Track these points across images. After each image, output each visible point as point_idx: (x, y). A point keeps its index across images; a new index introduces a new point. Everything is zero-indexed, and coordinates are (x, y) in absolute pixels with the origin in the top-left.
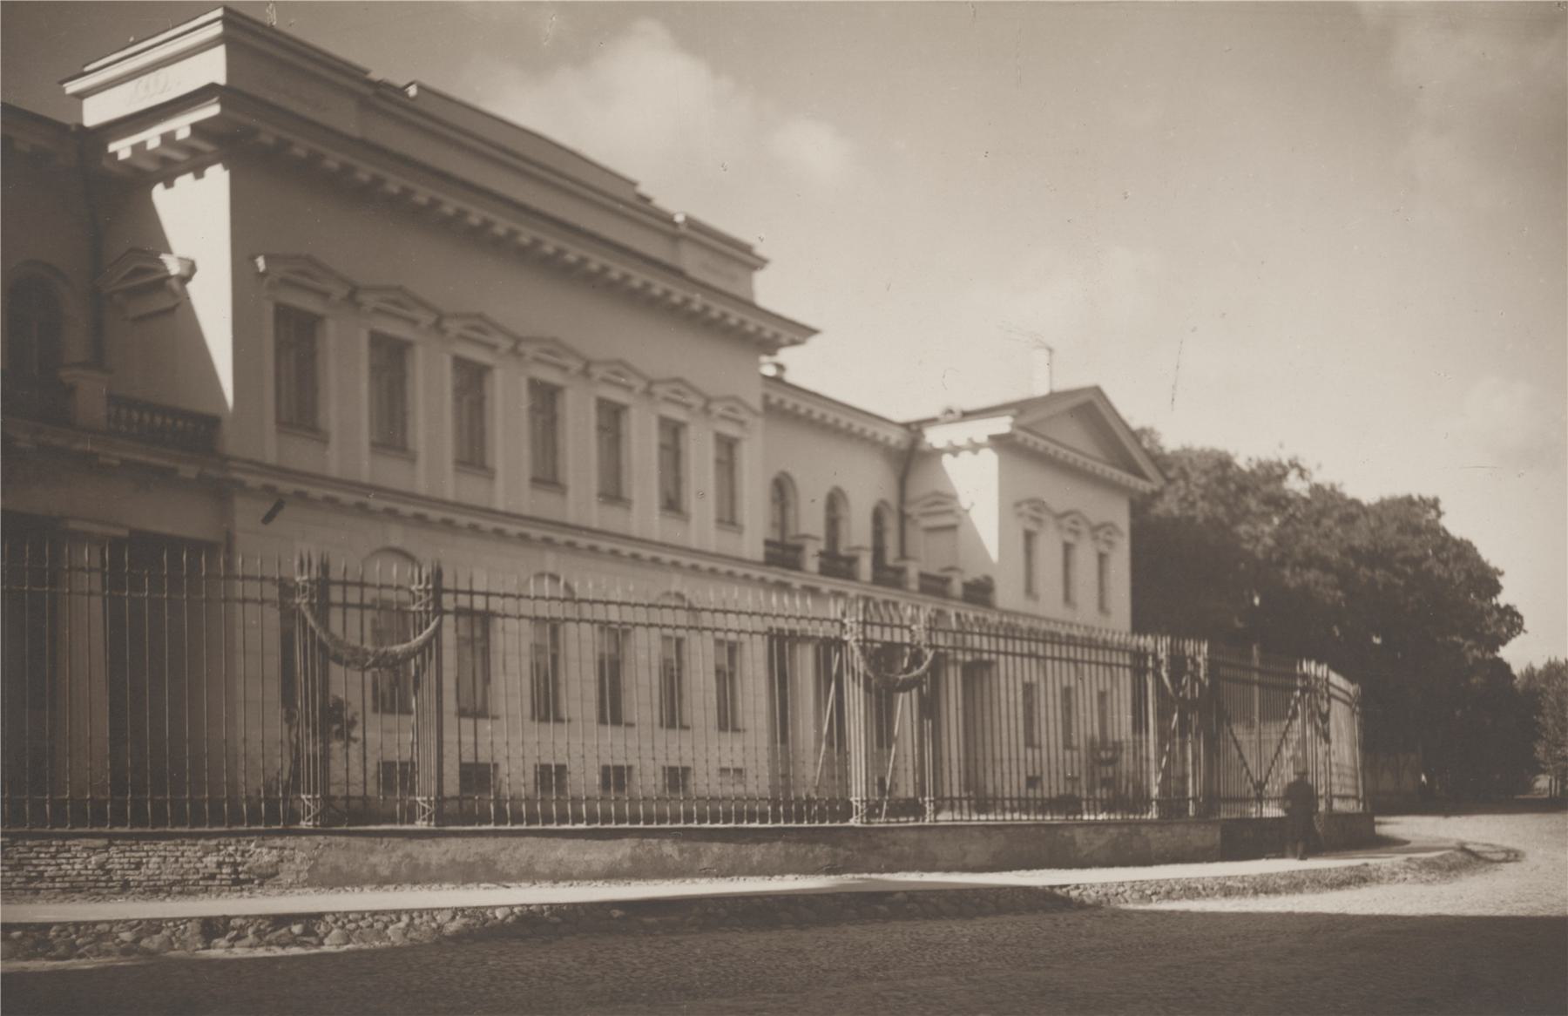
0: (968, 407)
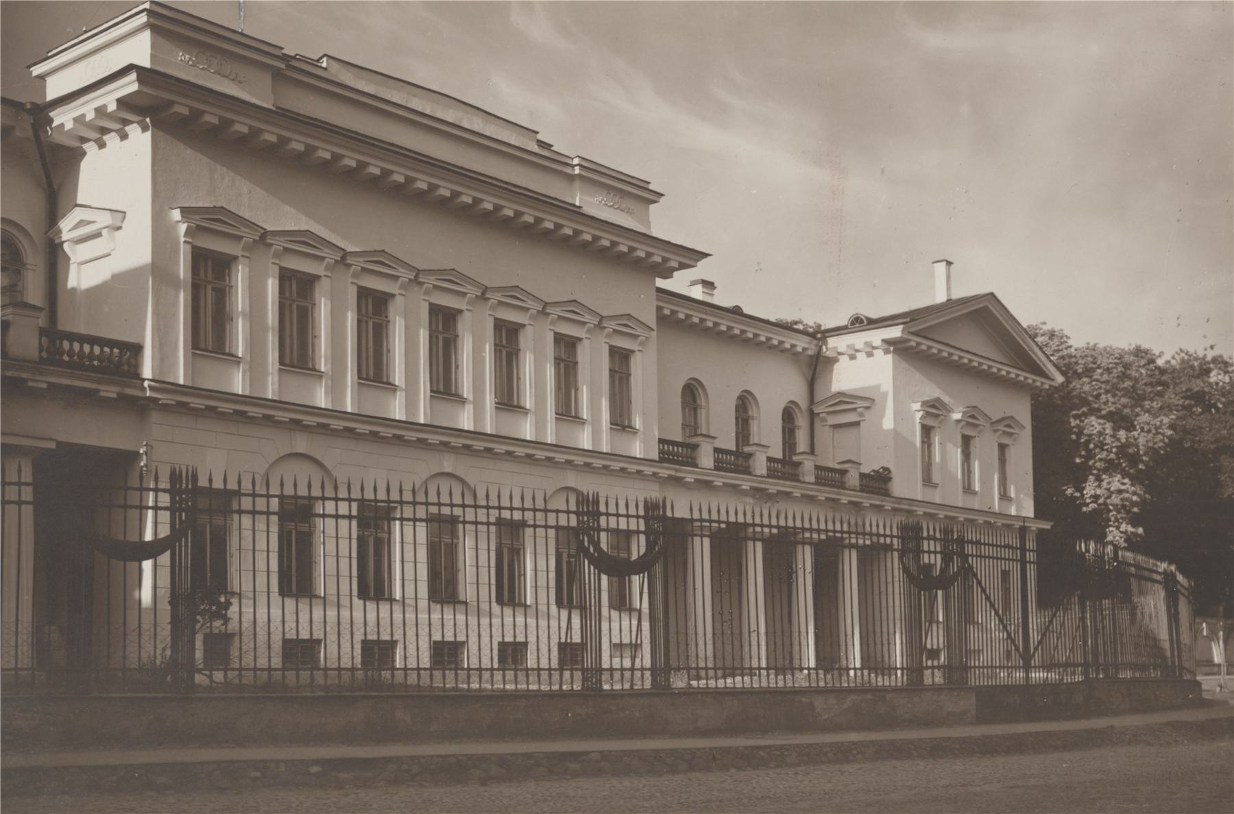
0: (874, 316)
